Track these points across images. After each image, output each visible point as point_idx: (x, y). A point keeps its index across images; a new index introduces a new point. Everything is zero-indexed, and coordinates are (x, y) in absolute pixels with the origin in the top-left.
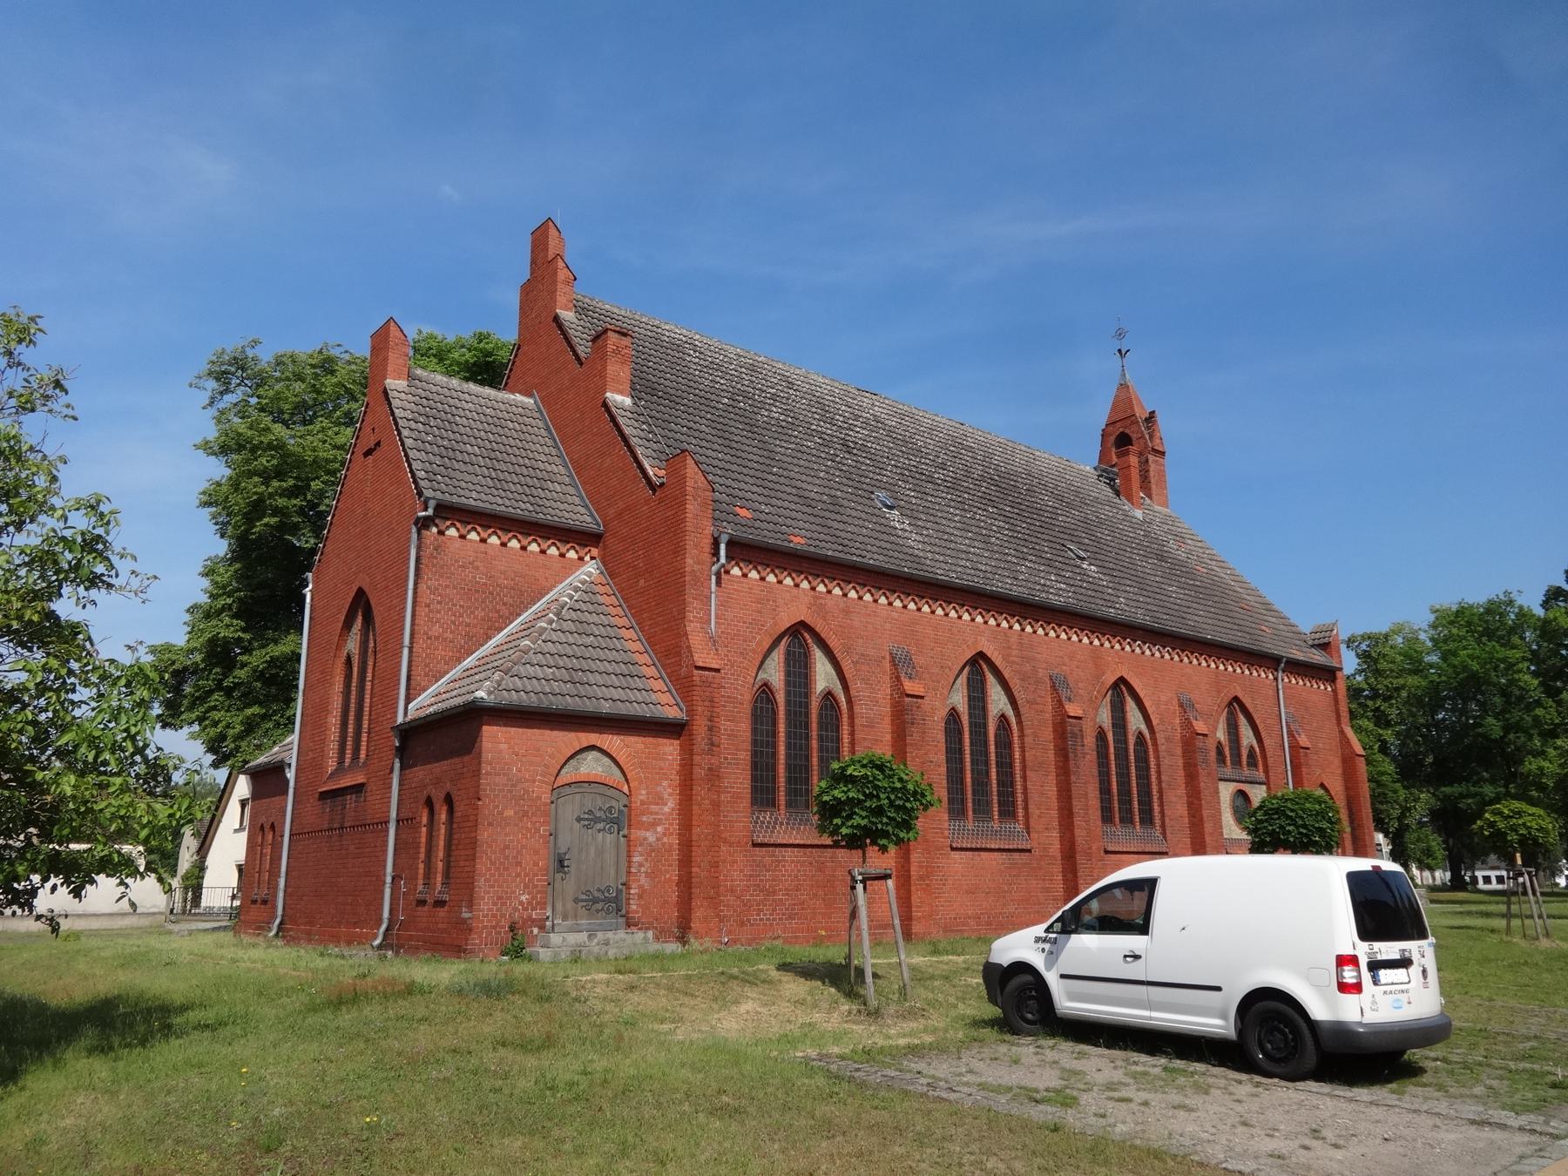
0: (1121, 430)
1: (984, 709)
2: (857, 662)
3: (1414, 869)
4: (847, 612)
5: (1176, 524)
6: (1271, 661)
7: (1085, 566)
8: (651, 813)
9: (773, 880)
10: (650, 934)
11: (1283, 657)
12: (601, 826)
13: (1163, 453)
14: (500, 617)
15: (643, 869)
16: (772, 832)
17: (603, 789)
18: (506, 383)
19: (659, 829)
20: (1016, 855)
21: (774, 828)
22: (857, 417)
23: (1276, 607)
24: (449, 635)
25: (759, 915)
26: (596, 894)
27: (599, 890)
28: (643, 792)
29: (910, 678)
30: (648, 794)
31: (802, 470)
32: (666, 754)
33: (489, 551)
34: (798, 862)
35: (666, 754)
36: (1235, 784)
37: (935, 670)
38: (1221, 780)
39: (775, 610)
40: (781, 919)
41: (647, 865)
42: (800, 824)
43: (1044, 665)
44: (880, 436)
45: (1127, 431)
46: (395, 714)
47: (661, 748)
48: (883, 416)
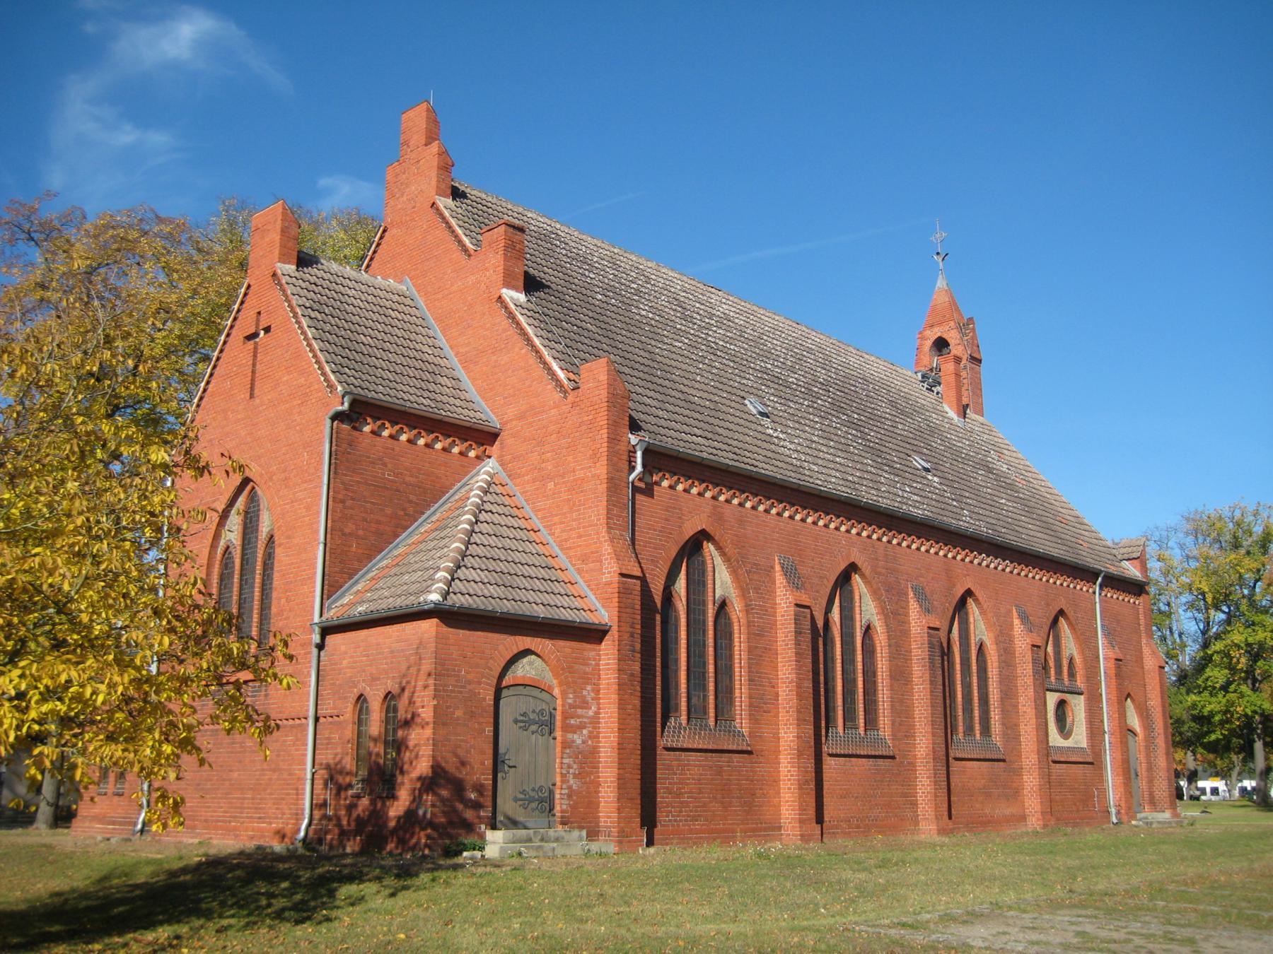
0: (939, 334)
1: (852, 619)
2: (750, 571)
3: (452, 831)
4: (741, 522)
5: (994, 434)
6: (1086, 574)
7: (930, 477)
8: (579, 717)
9: (680, 783)
10: (584, 833)
11: (1101, 571)
12: (534, 728)
13: (980, 361)
14: (406, 514)
15: (571, 771)
16: (679, 737)
17: (536, 692)
18: (368, 266)
19: (585, 732)
20: (880, 762)
21: (680, 732)
22: (711, 316)
23: (1086, 521)
24: (361, 532)
25: (668, 816)
26: (533, 794)
27: (533, 790)
28: (571, 696)
29: (797, 588)
30: (575, 697)
31: (682, 373)
32: (590, 659)
33: (397, 449)
34: (700, 766)
35: (590, 659)
36: (1058, 694)
37: (815, 580)
38: (1048, 690)
39: (680, 518)
40: (686, 821)
41: (575, 766)
42: (701, 730)
43: (905, 577)
44: (734, 336)
45: (945, 336)
46: (312, 614)
47: (585, 653)
48: (732, 314)
